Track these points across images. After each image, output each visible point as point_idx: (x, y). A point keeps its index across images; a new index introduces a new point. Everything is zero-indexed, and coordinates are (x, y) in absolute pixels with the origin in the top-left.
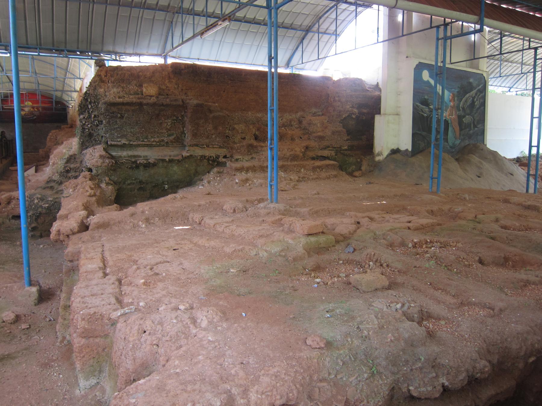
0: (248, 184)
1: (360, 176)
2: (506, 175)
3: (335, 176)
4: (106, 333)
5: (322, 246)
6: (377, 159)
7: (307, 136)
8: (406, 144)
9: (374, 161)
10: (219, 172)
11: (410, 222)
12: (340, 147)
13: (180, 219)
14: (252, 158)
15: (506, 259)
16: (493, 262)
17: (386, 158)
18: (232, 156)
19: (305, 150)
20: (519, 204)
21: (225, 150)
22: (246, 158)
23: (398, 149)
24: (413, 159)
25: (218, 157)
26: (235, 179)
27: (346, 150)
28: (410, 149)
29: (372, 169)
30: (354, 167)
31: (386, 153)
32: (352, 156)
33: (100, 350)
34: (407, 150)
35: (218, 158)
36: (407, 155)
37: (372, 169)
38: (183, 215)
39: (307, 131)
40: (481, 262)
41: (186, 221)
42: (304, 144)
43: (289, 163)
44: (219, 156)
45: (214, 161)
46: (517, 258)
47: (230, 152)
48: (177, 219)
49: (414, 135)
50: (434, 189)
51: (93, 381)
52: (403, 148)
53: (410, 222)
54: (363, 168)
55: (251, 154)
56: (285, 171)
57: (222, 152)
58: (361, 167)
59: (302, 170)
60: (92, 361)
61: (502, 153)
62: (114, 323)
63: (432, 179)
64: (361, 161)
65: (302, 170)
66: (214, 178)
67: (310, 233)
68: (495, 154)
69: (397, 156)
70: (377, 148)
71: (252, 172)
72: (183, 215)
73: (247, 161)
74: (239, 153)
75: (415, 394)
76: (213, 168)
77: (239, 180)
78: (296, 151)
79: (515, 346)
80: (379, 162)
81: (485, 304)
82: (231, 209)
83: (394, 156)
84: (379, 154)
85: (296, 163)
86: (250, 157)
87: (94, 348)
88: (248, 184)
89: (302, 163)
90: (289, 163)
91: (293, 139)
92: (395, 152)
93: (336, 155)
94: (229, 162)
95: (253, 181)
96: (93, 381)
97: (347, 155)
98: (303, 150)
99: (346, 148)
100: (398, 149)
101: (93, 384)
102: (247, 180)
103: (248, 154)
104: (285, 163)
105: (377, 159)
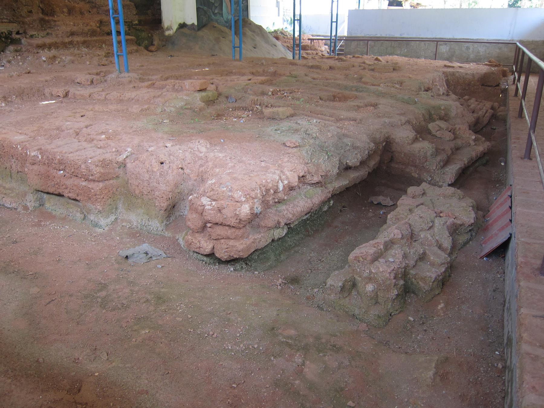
0: (57, 62)
1: (157, 51)
2: (272, 46)
3: (137, 51)
4: (117, 175)
5: (211, 99)
6: (167, 33)
7: (95, 10)
8: (191, 18)
9: (164, 36)
10: (16, 51)
11: (250, 80)
12: (131, 22)
13: (36, 95)
14: (48, 34)
15: (334, 97)
16: (328, 99)
17: (176, 32)
18: (25, 32)
19: (100, 25)
20: (304, 66)
21: (15, 24)
22: (42, 34)
23: (184, 23)
24: (200, 33)
25: (10, 33)
26: (40, 57)
27: (136, 25)
28: (196, 24)
29: (164, 43)
30: (146, 42)
31: (175, 27)
32: (144, 31)
33: (114, 189)
34: (193, 24)
35: (11, 35)
36: (194, 29)
37: (164, 43)
38: (39, 90)
39: (94, 5)
40: (321, 99)
41: (43, 97)
42: (98, 18)
43: (89, 39)
44: (12, 32)
45: (6, 38)
46: (340, 95)
47: (22, 27)
48: (34, 96)
49: (198, 9)
50: (237, 57)
51: (113, 218)
52: (189, 22)
53: (250, 80)
54: (156, 43)
55: (45, 30)
56: (87, 47)
57: (14, 27)
58: (152, 42)
59: (104, 46)
60: (109, 200)
61: (265, 27)
62: (123, 165)
63: (234, 48)
64: (152, 36)
65: (104, 46)
66: (14, 57)
67: (202, 88)
68: (260, 28)
69: (185, 30)
70: (166, 23)
71: (55, 49)
72: (39, 90)
73: (43, 37)
74: (32, 28)
75: (350, 164)
76: (8, 46)
77: (46, 58)
78: (91, 26)
79: (378, 136)
80: (170, 37)
81: (350, 118)
82: (88, 80)
83: (182, 30)
84: (169, 29)
85: (95, 38)
86: (45, 33)
87: (110, 189)
88: (57, 62)
89: (101, 38)
90: (89, 39)
91: (82, 13)
92: (183, 26)
93: (129, 30)
94: (25, 39)
95: (61, 58)
96: (113, 218)
97: (139, 30)
98: (98, 25)
99: (137, 22)
100: (184, 23)
101: (113, 220)
102: (55, 57)
103: (42, 30)
104: (86, 39)
105: (167, 33)
